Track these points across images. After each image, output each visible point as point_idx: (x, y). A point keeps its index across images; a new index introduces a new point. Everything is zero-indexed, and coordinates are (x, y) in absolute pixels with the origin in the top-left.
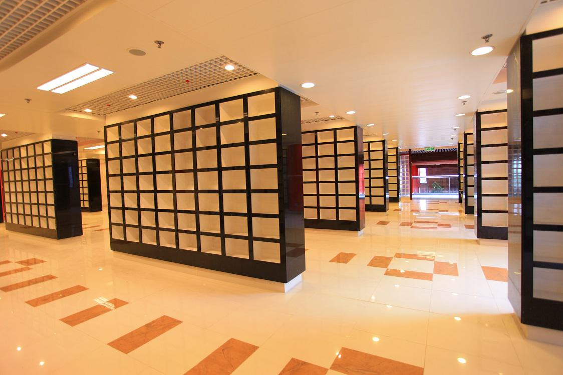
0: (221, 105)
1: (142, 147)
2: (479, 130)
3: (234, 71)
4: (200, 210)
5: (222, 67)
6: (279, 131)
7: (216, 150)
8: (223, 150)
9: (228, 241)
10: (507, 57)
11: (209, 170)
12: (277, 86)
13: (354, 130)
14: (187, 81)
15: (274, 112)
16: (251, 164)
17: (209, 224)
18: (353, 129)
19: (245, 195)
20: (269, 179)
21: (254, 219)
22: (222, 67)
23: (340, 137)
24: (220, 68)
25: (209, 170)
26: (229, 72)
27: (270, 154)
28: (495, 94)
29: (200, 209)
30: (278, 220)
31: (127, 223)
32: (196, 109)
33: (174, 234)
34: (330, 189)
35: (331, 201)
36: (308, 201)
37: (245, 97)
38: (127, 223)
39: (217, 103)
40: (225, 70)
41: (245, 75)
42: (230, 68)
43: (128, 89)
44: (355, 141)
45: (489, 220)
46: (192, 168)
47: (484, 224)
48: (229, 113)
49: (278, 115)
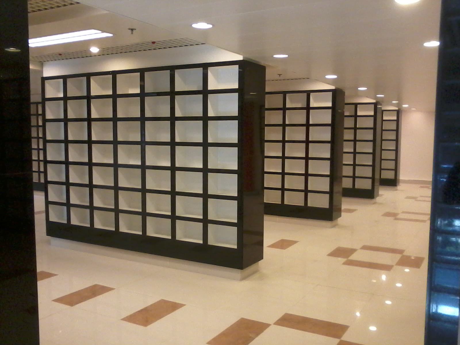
28: (309, 78)
31: (177, 214)
32: (146, 73)
33: (113, 214)
34: (299, 167)
35: (298, 183)
36: (270, 181)
38: (177, 214)
39: (172, 69)
46: (112, 116)
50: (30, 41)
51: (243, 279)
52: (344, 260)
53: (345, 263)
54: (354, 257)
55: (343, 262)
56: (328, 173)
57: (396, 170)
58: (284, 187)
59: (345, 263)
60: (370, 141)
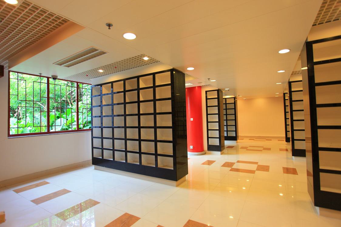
0: (156, 75)
1: (104, 100)
2: (291, 92)
3: (148, 60)
4: (127, 138)
5: (141, 58)
6: (173, 93)
7: (153, 102)
8: (141, 104)
9: (159, 158)
10: (299, 53)
11: (108, 116)
12: (171, 68)
13: (124, 105)
14: (116, 67)
15: (170, 83)
16: (157, 112)
17: (132, 146)
18: (217, 91)
19: (153, 129)
20: (167, 120)
21: (142, 142)
22: (141, 58)
23: (210, 96)
24: (141, 59)
25: (108, 116)
26: (145, 61)
27: (167, 107)
29: (104, 137)
30: (172, 144)
37: (154, 74)
40: (143, 60)
41: (144, 65)
42: (146, 59)
43: (106, 66)
44: (218, 98)
45: (299, 146)
47: (296, 148)
48: (145, 82)
49: (172, 84)
50: (186, 84)
51: (177, 186)
52: (246, 149)
53: (230, 170)
54: (248, 149)
55: (230, 170)
56: (218, 129)
57: (236, 131)
58: (157, 139)
59: (230, 170)
60: (169, 99)
